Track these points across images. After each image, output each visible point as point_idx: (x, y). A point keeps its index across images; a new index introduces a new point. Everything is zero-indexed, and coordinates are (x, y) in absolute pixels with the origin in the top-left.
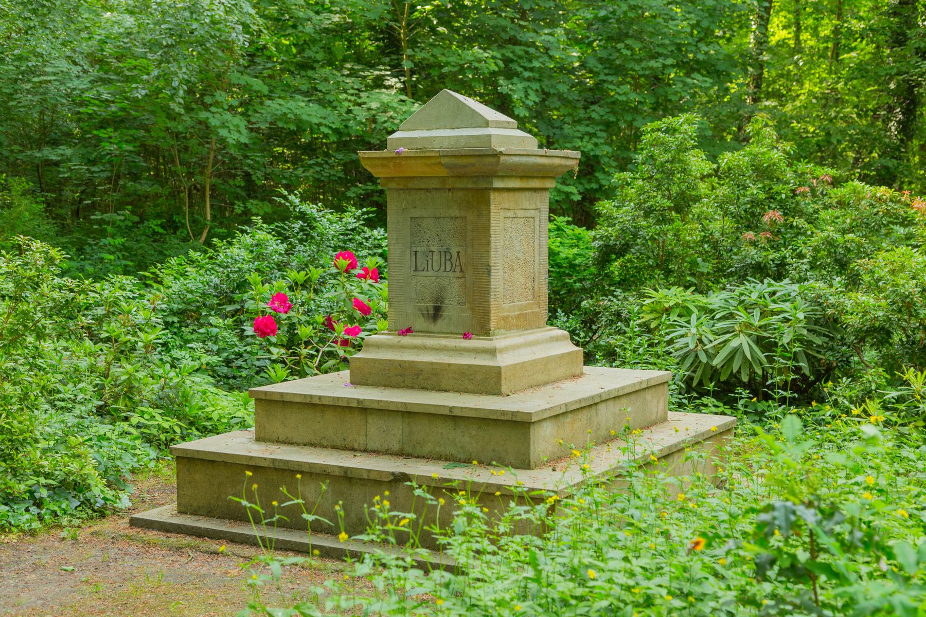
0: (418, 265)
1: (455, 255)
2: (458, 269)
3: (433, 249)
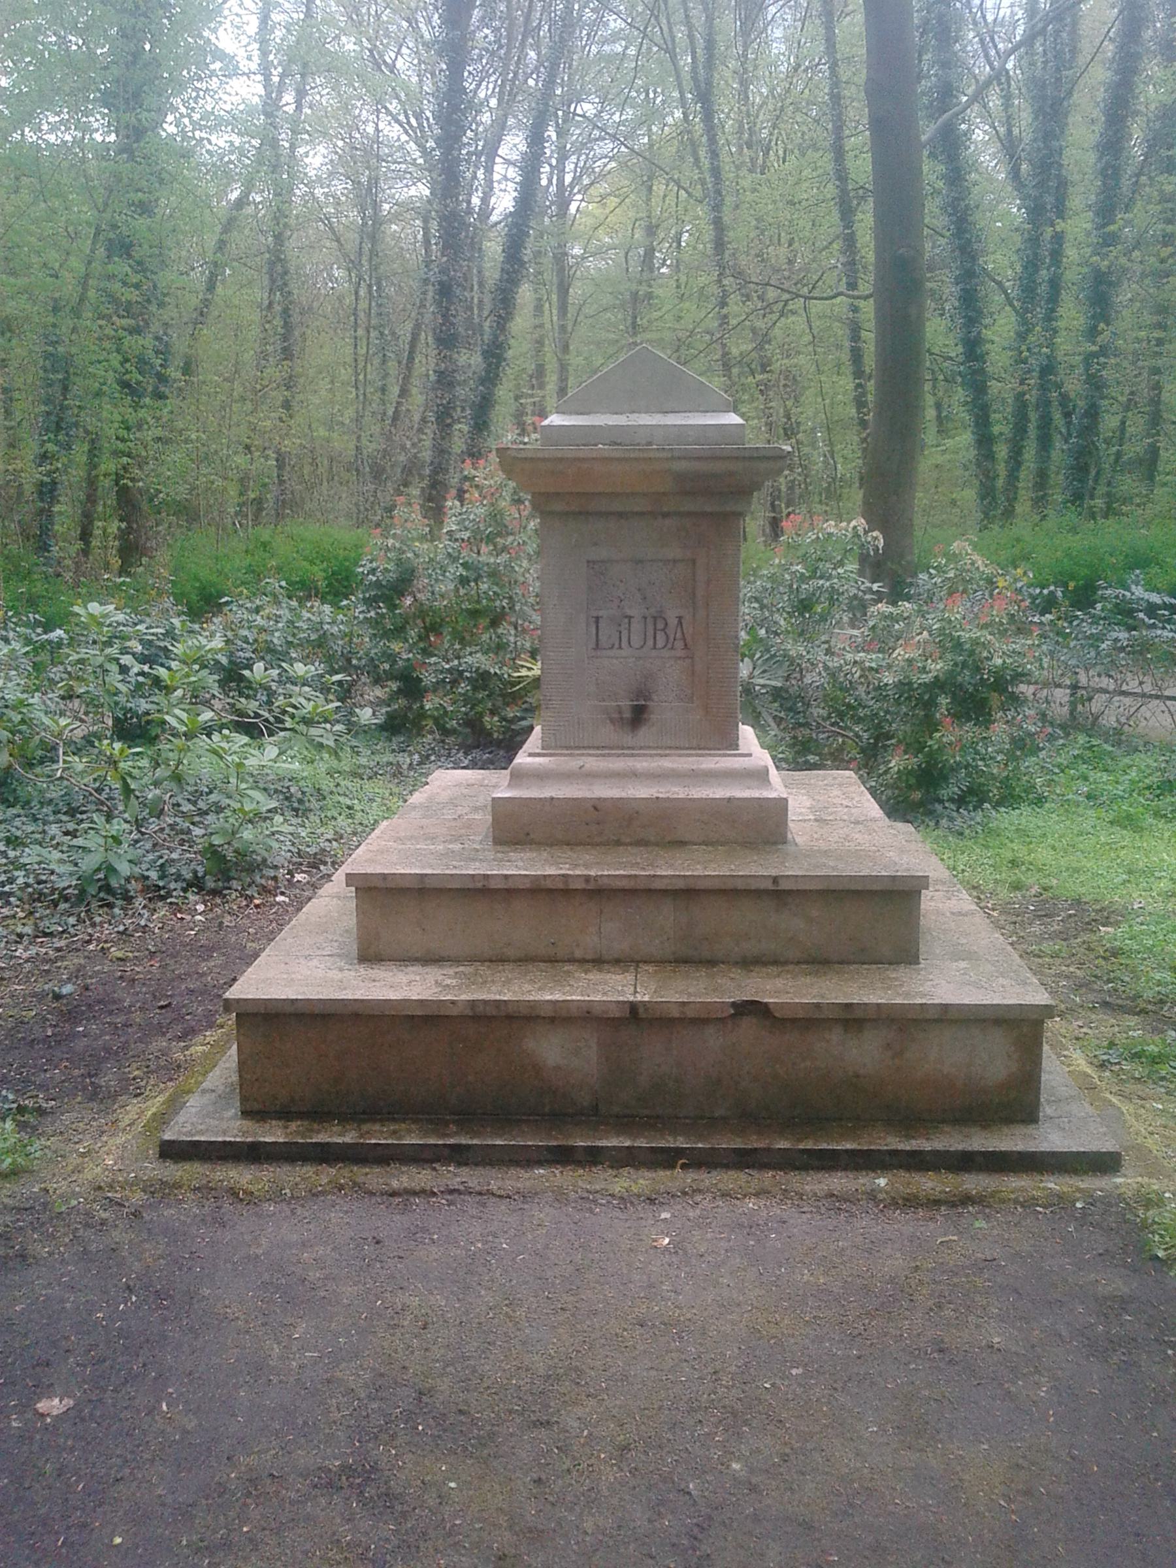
0: (603, 638)
1: (673, 622)
2: (679, 644)
3: (629, 612)
